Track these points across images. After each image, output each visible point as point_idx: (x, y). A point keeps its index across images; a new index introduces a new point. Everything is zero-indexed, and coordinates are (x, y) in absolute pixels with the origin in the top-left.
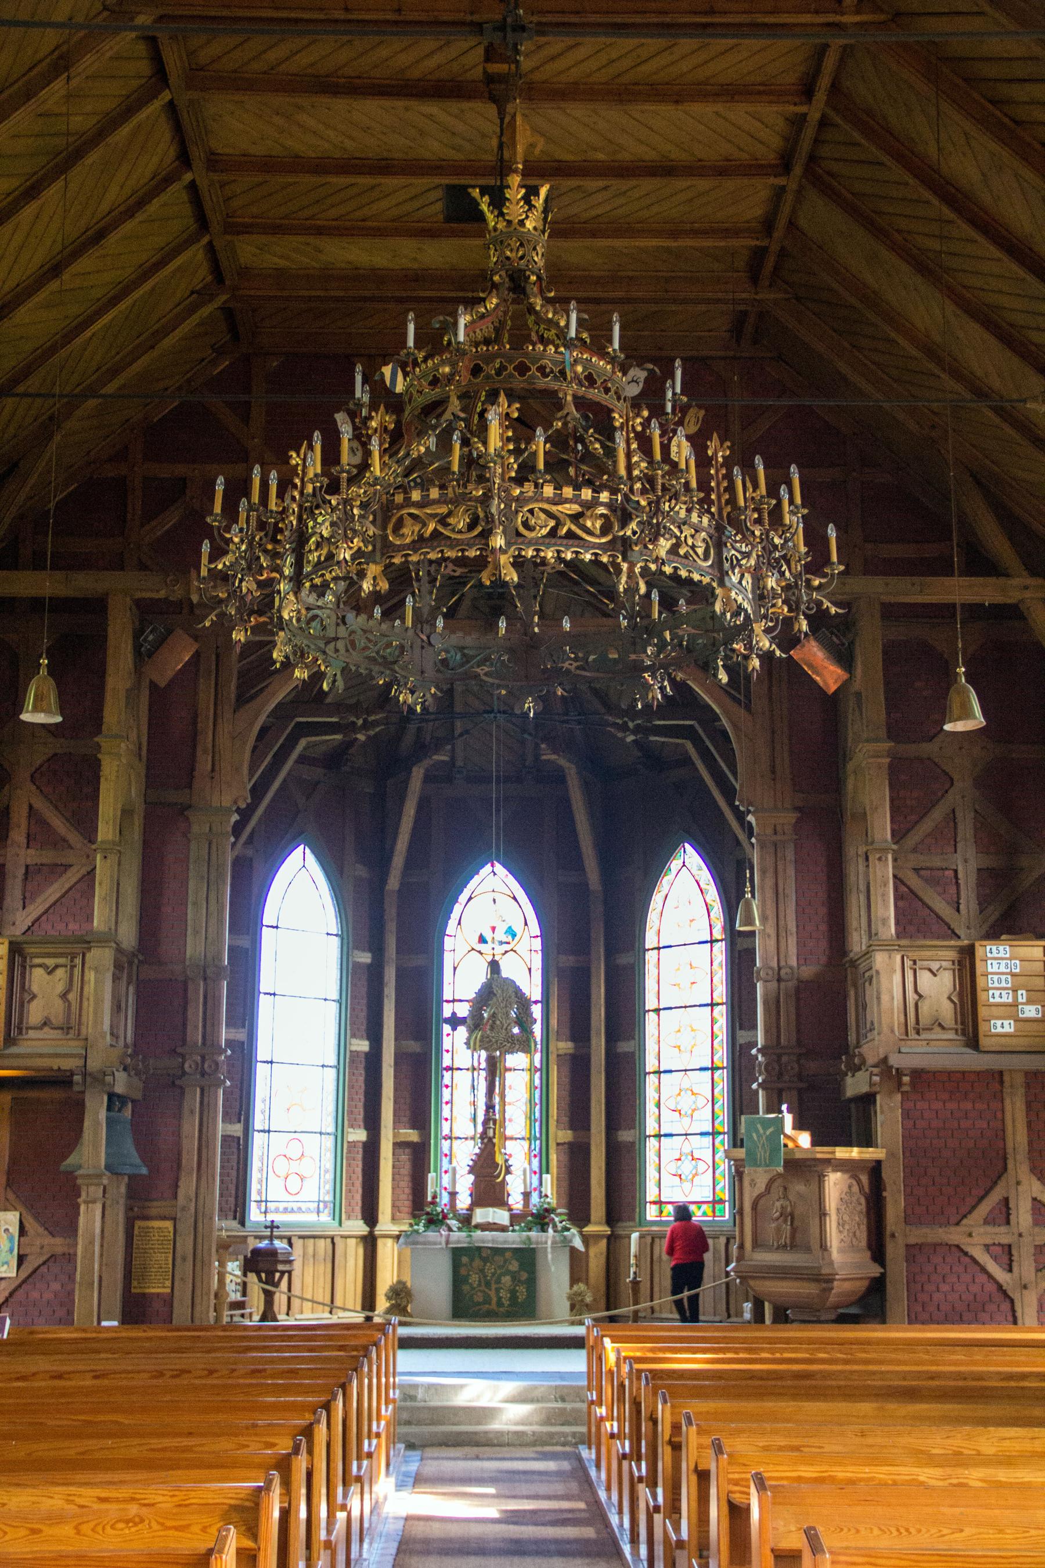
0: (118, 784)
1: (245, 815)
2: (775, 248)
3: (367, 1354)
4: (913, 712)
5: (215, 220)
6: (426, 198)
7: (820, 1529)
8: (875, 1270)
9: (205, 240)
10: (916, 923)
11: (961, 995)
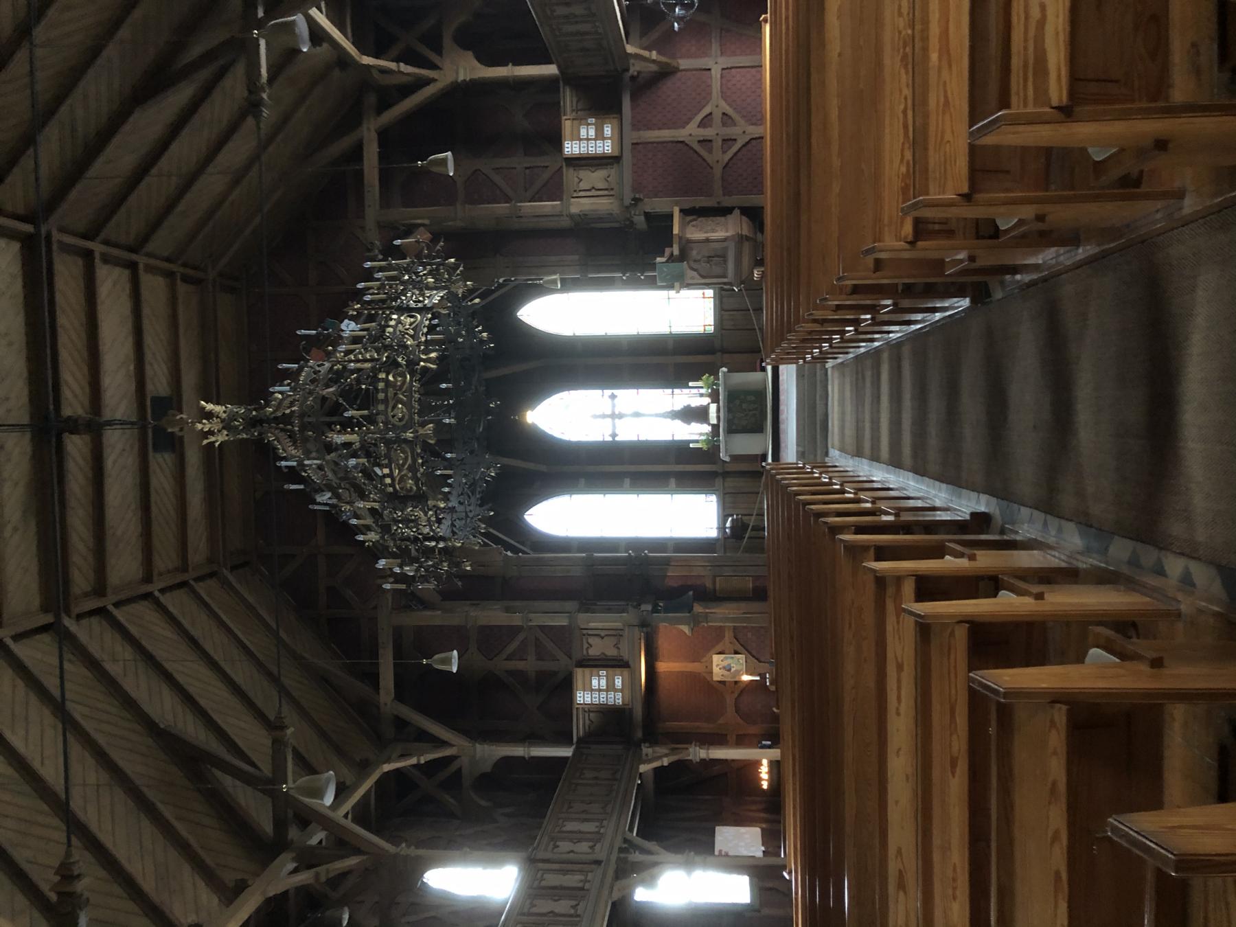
0: (493, 615)
1: (508, 547)
2: (181, 269)
3: (778, 481)
4: (443, 190)
5: (180, 578)
6: (161, 463)
7: (186, 440)
8: (737, 212)
9: (192, 582)
10: (554, 189)
11: (592, 166)
